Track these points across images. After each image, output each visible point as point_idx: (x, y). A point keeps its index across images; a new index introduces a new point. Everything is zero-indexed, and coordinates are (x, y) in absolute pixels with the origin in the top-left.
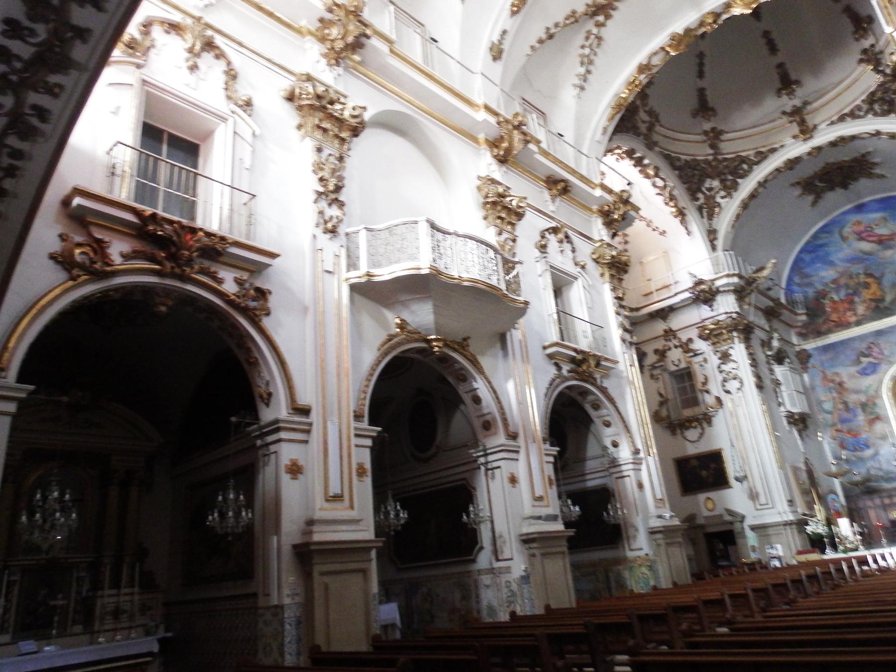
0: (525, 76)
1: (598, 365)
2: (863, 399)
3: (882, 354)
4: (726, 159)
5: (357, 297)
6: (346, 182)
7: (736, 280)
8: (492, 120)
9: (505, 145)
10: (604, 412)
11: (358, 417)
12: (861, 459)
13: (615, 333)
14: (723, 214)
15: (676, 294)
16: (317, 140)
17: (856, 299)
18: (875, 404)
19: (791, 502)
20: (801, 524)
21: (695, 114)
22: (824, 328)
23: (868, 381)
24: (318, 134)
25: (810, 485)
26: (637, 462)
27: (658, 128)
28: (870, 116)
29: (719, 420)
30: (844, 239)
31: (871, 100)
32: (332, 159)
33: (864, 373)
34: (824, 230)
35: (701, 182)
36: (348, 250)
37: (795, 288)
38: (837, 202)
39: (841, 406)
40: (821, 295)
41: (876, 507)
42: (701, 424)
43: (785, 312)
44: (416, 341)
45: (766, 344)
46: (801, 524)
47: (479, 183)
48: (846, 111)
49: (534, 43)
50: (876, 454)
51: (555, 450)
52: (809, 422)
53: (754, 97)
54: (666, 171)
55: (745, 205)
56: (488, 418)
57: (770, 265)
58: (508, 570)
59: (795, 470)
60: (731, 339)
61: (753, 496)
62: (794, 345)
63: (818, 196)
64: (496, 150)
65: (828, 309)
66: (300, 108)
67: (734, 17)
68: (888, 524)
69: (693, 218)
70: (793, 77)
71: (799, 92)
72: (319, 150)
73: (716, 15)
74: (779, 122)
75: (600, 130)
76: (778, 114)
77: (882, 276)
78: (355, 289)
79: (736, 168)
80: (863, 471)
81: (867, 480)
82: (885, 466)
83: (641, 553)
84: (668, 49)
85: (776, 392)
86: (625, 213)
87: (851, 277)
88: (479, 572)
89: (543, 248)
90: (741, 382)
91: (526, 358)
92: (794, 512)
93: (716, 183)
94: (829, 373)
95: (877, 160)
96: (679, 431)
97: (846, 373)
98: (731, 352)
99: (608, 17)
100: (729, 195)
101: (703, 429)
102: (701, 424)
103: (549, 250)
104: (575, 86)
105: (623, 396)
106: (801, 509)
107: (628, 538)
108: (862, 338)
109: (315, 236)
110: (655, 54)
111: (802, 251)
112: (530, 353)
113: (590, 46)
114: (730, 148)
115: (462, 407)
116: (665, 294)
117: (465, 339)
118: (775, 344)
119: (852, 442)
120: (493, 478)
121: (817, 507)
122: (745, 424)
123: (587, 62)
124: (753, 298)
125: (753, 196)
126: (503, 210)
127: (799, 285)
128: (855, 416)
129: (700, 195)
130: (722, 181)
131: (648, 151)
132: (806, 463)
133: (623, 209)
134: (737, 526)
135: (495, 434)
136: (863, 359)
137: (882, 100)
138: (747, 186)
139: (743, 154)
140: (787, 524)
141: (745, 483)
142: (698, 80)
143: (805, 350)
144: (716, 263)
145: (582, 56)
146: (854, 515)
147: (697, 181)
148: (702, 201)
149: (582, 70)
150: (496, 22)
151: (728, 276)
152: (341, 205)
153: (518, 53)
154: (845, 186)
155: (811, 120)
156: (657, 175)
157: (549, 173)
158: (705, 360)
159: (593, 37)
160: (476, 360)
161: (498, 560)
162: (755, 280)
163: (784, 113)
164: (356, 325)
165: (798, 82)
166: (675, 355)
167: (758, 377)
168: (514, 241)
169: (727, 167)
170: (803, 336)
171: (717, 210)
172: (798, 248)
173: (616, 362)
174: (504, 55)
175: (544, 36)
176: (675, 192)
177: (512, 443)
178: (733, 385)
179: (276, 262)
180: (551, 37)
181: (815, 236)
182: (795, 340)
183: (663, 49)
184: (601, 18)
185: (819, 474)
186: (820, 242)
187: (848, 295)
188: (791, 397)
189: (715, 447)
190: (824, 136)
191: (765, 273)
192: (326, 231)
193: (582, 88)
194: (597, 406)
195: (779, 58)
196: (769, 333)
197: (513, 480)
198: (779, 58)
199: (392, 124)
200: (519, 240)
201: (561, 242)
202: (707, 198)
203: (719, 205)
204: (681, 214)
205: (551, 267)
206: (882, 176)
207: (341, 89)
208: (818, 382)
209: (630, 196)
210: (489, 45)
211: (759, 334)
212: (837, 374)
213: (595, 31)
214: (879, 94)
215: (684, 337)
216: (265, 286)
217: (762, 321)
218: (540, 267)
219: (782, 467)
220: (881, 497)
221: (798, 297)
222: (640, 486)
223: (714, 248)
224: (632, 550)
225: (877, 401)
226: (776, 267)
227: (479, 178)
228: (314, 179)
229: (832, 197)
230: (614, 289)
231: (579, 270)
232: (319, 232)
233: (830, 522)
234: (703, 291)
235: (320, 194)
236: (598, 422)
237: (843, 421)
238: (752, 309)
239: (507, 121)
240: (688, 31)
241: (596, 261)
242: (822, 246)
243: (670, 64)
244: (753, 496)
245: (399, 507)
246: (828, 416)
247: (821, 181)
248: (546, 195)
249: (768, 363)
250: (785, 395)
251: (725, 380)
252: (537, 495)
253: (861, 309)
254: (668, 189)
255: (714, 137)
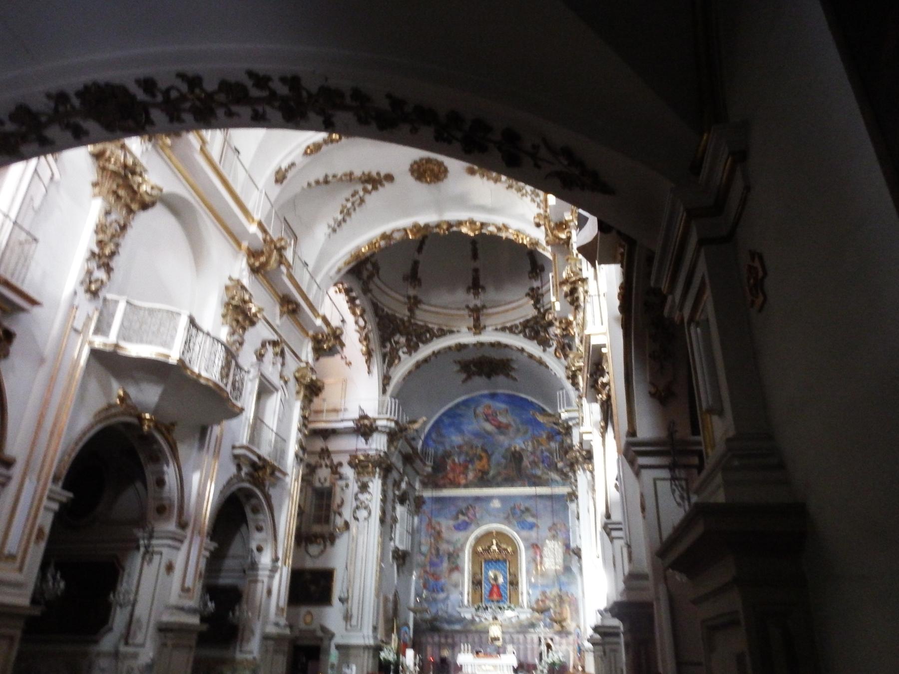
0: (293, 203)
1: (272, 473)
2: (451, 549)
3: (475, 515)
4: (416, 324)
5: (96, 366)
6: (121, 250)
7: (393, 425)
8: (260, 236)
9: (263, 259)
10: (261, 517)
11: (55, 479)
12: (435, 600)
13: (292, 448)
14: (401, 365)
15: (342, 421)
16: (109, 203)
17: (470, 466)
18: (458, 556)
19: (375, 629)
20: (377, 649)
21: (405, 278)
22: (441, 482)
23: (458, 536)
24: (112, 199)
25: (391, 616)
26: (274, 570)
27: (376, 279)
28: (521, 335)
29: (342, 543)
30: (476, 415)
31: (526, 324)
32: (115, 225)
33: (458, 528)
34: (465, 403)
35: (393, 334)
36: (101, 314)
37: (431, 442)
38: (480, 386)
39: (433, 551)
40: (447, 455)
41: (434, 644)
42: (325, 542)
43: (418, 461)
44: (130, 415)
45: (397, 484)
46: (377, 649)
47: (228, 283)
48: (508, 325)
49: (312, 180)
50: (447, 598)
51: (213, 546)
52: (408, 559)
53: (452, 287)
54: (370, 315)
55: (418, 365)
56: (166, 503)
57: (421, 421)
58: (135, 656)
59: (386, 599)
60: (374, 474)
61: (347, 617)
62: (415, 489)
63: (469, 377)
64: (252, 260)
65: (448, 468)
66: (103, 169)
67: (460, 233)
68: (438, 660)
69: (377, 360)
70: (482, 283)
71: (482, 296)
72: (108, 213)
73: (450, 225)
74: (462, 312)
75: (335, 269)
76: (464, 306)
77: (492, 454)
78: (95, 353)
79: (421, 334)
80: (434, 611)
81: (435, 619)
82: (450, 610)
83: (249, 657)
84: (409, 232)
85: (392, 527)
86: (334, 346)
87: (472, 447)
88: (98, 654)
89: (260, 356)
90: (370, 514)
91: (217, 454)
92: (375, 638)
93: (403, 340)
94: (433, 521)
95: (515, 366)
96: (303, 544)
97: (445, 524)
98: (370, 484)
99: (375, 188)
100: (409, 353)
101: (325, 547)
102: (325, 542)
103: (289, 383)
104: (329, 226)
105: (281, 506)
106: (381, 635)
107: (242, 641)
108: (465, 499)
109: (75, 293)
110: (398, 230)
111: (444, 414)
112: (222, 449)
113: (353, 204)
114: (423, 317)
115: (139, 485)
116: (333, 417)
117: (173, 424)
118: (403, 486)
119: (433, 584)
120: (151, 560)
121: (394, 636)
122: (361, 554)
123: (346, 213)
124: (401, 443)
125: (426, 360)
126: (240, 314)
127: (434, 441)
128: (442, 562)
129: (388, 345)
130: (408, 340)
131: (362, 295)
132: (396, 595)
133: (333, 341)
134: (326, 642)
135: (168, 519)
136: (461, 517)
137: (532, 329)
138: (425, 351)
139: (430, 326)
140: (366, 648)
141: (346, 604)
142: (416, 253)
143: (422, 497)
144: (381, 404)
145: (344, 207)
146: (417, 646)
147: (391, 332)
148: (388, 349)
149: (340, 217)
150: (290, 153)
151: (388, 419)
152: (109, 270)
153: (296, 184)
154: (489, 376)
155: (484, 321)
156: (362, 316)
157: (285, 292)
158: (347, 486)
159: (357, 196)
160: (176, 446)
161: (127, 643)
162: (406, 429)
163: (468, 307)
164: (83, 387)
165: (483, 288)
166: (324, 473)
167: (384, 512)
168: (241, 344)
169: (415, 330)
170: (425, 485)
171: (396, 361)
172: (442, 411)
173: (285, 474)
174: (285, 182)
175: (321, 179)
176: (371, 335)
177: (179, 531)
178: (362, 514)
179: (36, 310)
180: (326, 182)
181: (457, 406)
182: (417, 485)
183: (405, 230)
184: (370, 187)
185: (402, 608)
186: (459, 412)
187: (466, 461)
188: (401, 535)
189: (330, 565)
190: (488, 337)
191: (416, 426)
192: (88, 290)
193: (334, 230)
194: (256, 510)
195: (477, 264)
196: (402, 476)
197: (170, 568)
198: (477, 264)
199: (175, 207)
200: (246, 345)
201: (276, 354)
202: (392, 348)
203: (400, 358)
204: (369, 354)
205: (262, 375)
206: (515, 379)
207: (143, 161)
208: (424, 526)
209: (342, 333)
210: (277, 168)
211: (395, 475)
212: (439, 524)
213: (361, 193)
214: (532, 323)
215: (336, 459)
216: (14, 328)
217: (399, 465)
218: (254, 372)
219: (377, 596)
220: (440, 637)
221: (431, 451)
222: (269, 592)
223: (384, 391)
224: (241, 651)
225: (460, 554)
226: (423, 424)
227: (230, 279)
228: (94, 238)
229: (478, 380)
230: (303, 408)
231: (282, 383)
232: (81, 290)
233: (400, 652)
234: (366, 426)
235: (93, 254)
236: (252, 525)
237: (432, 564)
238: (397, 453)
239: (272, 241)
240: (427, 226)
241: (297, 379)
242: (460, 415)
243: (405, 241)
244: (347, 617)
245: (58, 576)
246: (423, 558)
247: (474, 366)
248: (277, 309)
249: (394, 501)
250: (398, 532)
251: (357, 508)
252: (186, 585)
253: (471, 475)
254: (366, 330)
255: (414, 303)
